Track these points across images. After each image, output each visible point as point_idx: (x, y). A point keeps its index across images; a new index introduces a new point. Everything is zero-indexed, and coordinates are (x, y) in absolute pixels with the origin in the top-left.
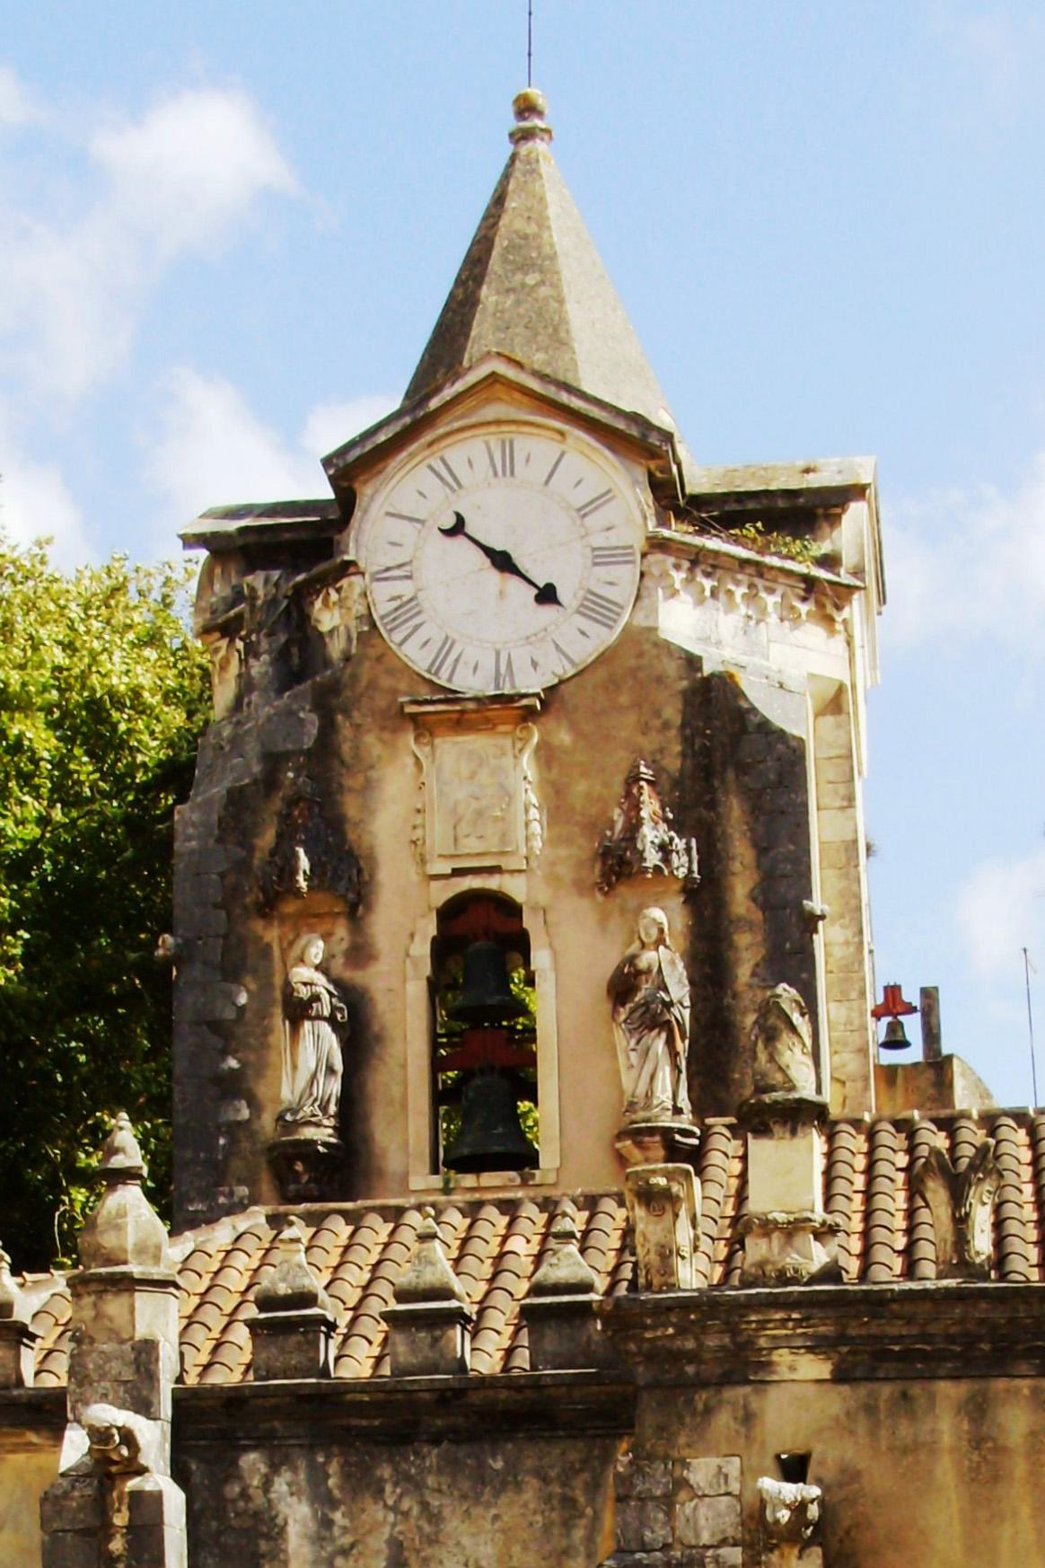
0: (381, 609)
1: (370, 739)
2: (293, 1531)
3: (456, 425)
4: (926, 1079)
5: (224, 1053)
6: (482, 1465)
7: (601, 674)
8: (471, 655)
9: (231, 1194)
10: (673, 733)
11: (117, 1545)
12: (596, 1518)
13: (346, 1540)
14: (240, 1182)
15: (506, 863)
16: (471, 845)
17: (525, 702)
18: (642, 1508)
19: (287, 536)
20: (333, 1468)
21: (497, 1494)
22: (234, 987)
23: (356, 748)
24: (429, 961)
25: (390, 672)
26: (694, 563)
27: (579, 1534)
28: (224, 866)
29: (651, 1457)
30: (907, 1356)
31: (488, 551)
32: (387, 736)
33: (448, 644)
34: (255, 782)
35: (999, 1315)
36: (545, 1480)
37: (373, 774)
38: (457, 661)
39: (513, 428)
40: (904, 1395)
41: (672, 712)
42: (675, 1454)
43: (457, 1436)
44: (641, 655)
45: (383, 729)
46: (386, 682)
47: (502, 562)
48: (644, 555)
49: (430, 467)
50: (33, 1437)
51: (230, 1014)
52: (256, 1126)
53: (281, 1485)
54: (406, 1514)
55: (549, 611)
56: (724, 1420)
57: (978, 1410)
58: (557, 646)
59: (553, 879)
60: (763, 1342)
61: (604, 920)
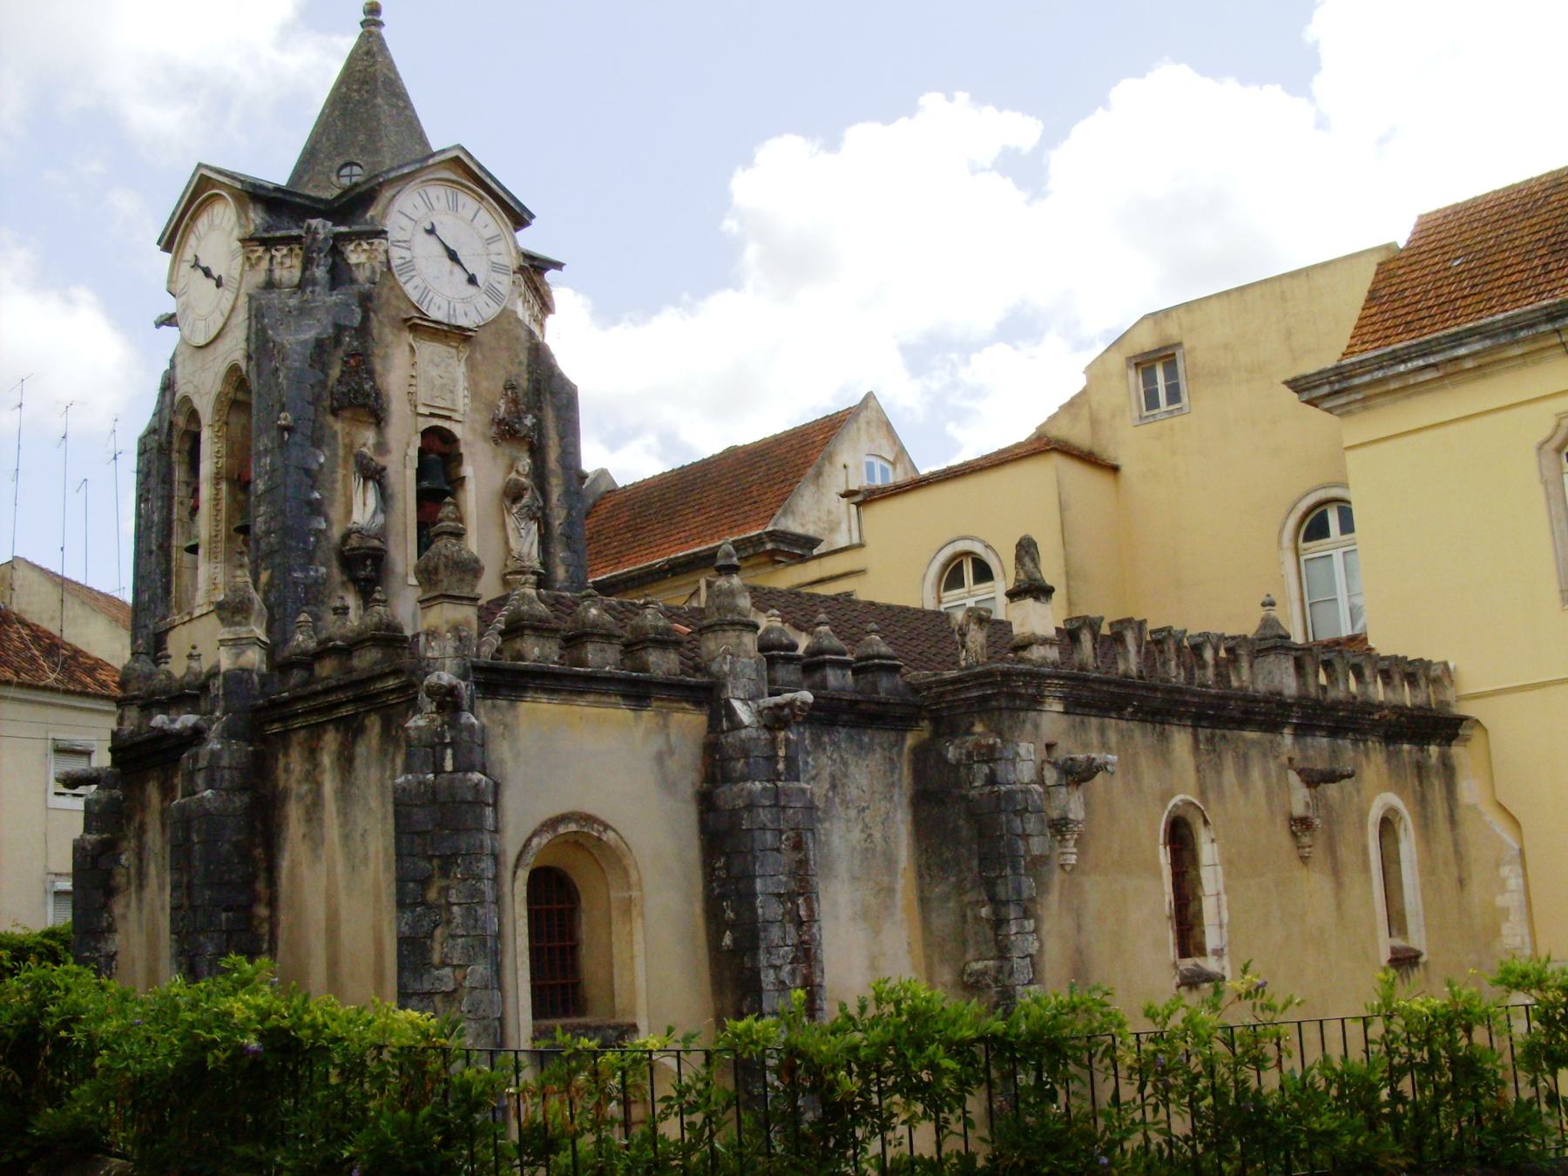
0: (395, 262)
1: (387, 330)
5: (312, 488)
6: (861, 740)
8: (437, 300)
9: (317, 571)
10: (524, 368)
11: (781, 766)
12: (901, 769)
13: (814, 772)
14: (322, 564)
15: (456, 416)
19: (298, 200)
20: (807, 735)
21: (867, 754)
22: (318, 452)
23: (381, 333)
25: (397, 297)
27: (896, 776)
28: (312, 381)
31: (447, 248)
32: (396, 331)
34: (329, 338)
36: (884, 749)
37: (389, 351)
40: (1082, 722)
44: (510, 323)
46: (394, 302)
50: (687, 706)
51: (315, 467)
52: (329, 534)
55: (471, 289)
56: (1028, 726)
57: (1102, 731)
61: (495, 457)
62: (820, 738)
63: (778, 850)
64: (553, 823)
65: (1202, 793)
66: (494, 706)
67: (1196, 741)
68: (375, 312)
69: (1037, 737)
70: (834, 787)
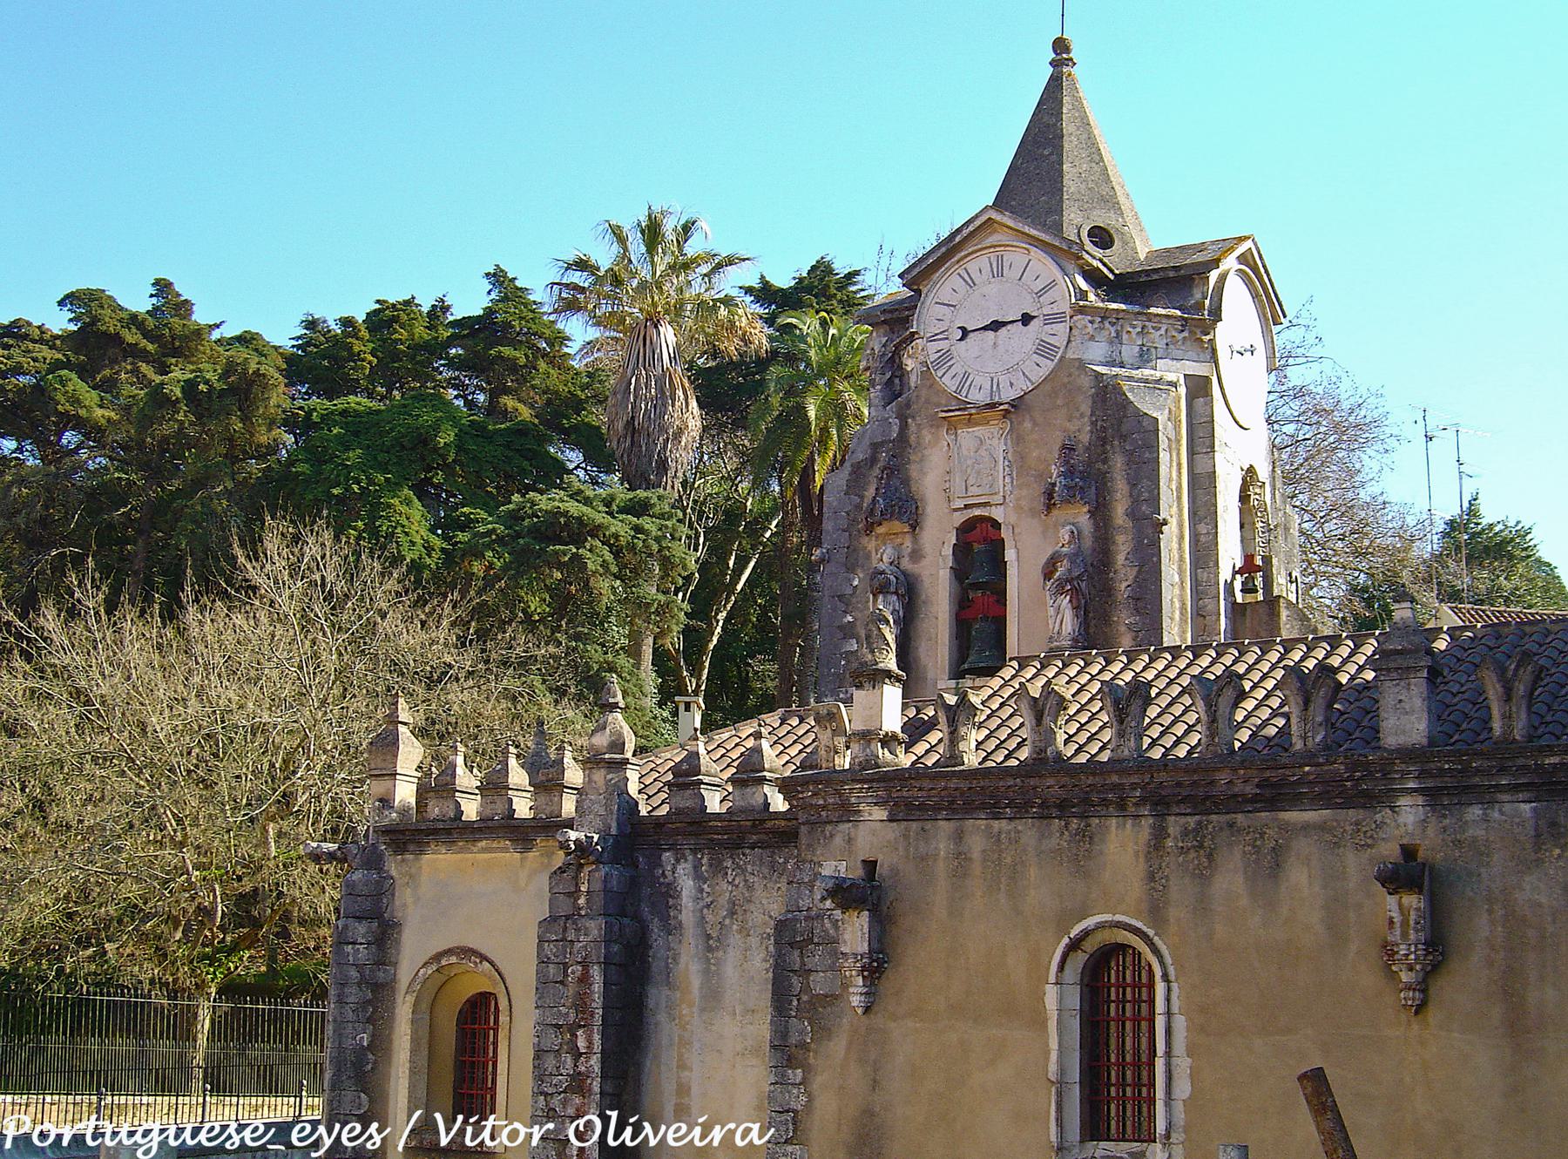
2: (685, 893)
3: (970, 250)
4: (1262, 610)
7: (1048, 387)
8: (979, 380)
11: (582, 901)
13: (709, 900)
16: (973, 490)
17: (1002, 407)
18: (799, 888)
24: (951, 558)
26: (1103, 318)
29: (804, 861)
30: (922, 807)
33: (966, 375)
35: (964, 785)
37: (926, 452)
38: (970, 385)
39: (1002, 248)
41: (1086, 408)
42: (815, 859)
43: (763, 845)
45: (932, 426)
47: (996, 326)
48: (1071, 317)
49: (959, 274)
51: (849, 591)
53: (680, 869)
54: (737, 886)
56: (838, 840)
57: (959, 837)
58: (1024, 374)
59: (1018, 508)
60: (853, 800)
62: (721, 862)
63: (561, 982)
64: (437, 957)
65: (1156, 912)
66: (403, 860)
67: (1159, 834)
68: (913, 418)
69: (850, 852)
70: (732, 913)
